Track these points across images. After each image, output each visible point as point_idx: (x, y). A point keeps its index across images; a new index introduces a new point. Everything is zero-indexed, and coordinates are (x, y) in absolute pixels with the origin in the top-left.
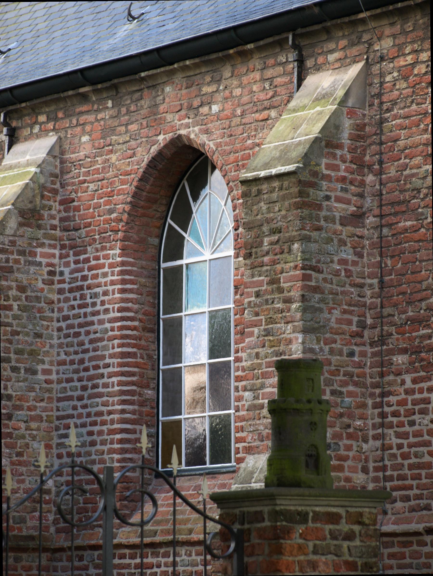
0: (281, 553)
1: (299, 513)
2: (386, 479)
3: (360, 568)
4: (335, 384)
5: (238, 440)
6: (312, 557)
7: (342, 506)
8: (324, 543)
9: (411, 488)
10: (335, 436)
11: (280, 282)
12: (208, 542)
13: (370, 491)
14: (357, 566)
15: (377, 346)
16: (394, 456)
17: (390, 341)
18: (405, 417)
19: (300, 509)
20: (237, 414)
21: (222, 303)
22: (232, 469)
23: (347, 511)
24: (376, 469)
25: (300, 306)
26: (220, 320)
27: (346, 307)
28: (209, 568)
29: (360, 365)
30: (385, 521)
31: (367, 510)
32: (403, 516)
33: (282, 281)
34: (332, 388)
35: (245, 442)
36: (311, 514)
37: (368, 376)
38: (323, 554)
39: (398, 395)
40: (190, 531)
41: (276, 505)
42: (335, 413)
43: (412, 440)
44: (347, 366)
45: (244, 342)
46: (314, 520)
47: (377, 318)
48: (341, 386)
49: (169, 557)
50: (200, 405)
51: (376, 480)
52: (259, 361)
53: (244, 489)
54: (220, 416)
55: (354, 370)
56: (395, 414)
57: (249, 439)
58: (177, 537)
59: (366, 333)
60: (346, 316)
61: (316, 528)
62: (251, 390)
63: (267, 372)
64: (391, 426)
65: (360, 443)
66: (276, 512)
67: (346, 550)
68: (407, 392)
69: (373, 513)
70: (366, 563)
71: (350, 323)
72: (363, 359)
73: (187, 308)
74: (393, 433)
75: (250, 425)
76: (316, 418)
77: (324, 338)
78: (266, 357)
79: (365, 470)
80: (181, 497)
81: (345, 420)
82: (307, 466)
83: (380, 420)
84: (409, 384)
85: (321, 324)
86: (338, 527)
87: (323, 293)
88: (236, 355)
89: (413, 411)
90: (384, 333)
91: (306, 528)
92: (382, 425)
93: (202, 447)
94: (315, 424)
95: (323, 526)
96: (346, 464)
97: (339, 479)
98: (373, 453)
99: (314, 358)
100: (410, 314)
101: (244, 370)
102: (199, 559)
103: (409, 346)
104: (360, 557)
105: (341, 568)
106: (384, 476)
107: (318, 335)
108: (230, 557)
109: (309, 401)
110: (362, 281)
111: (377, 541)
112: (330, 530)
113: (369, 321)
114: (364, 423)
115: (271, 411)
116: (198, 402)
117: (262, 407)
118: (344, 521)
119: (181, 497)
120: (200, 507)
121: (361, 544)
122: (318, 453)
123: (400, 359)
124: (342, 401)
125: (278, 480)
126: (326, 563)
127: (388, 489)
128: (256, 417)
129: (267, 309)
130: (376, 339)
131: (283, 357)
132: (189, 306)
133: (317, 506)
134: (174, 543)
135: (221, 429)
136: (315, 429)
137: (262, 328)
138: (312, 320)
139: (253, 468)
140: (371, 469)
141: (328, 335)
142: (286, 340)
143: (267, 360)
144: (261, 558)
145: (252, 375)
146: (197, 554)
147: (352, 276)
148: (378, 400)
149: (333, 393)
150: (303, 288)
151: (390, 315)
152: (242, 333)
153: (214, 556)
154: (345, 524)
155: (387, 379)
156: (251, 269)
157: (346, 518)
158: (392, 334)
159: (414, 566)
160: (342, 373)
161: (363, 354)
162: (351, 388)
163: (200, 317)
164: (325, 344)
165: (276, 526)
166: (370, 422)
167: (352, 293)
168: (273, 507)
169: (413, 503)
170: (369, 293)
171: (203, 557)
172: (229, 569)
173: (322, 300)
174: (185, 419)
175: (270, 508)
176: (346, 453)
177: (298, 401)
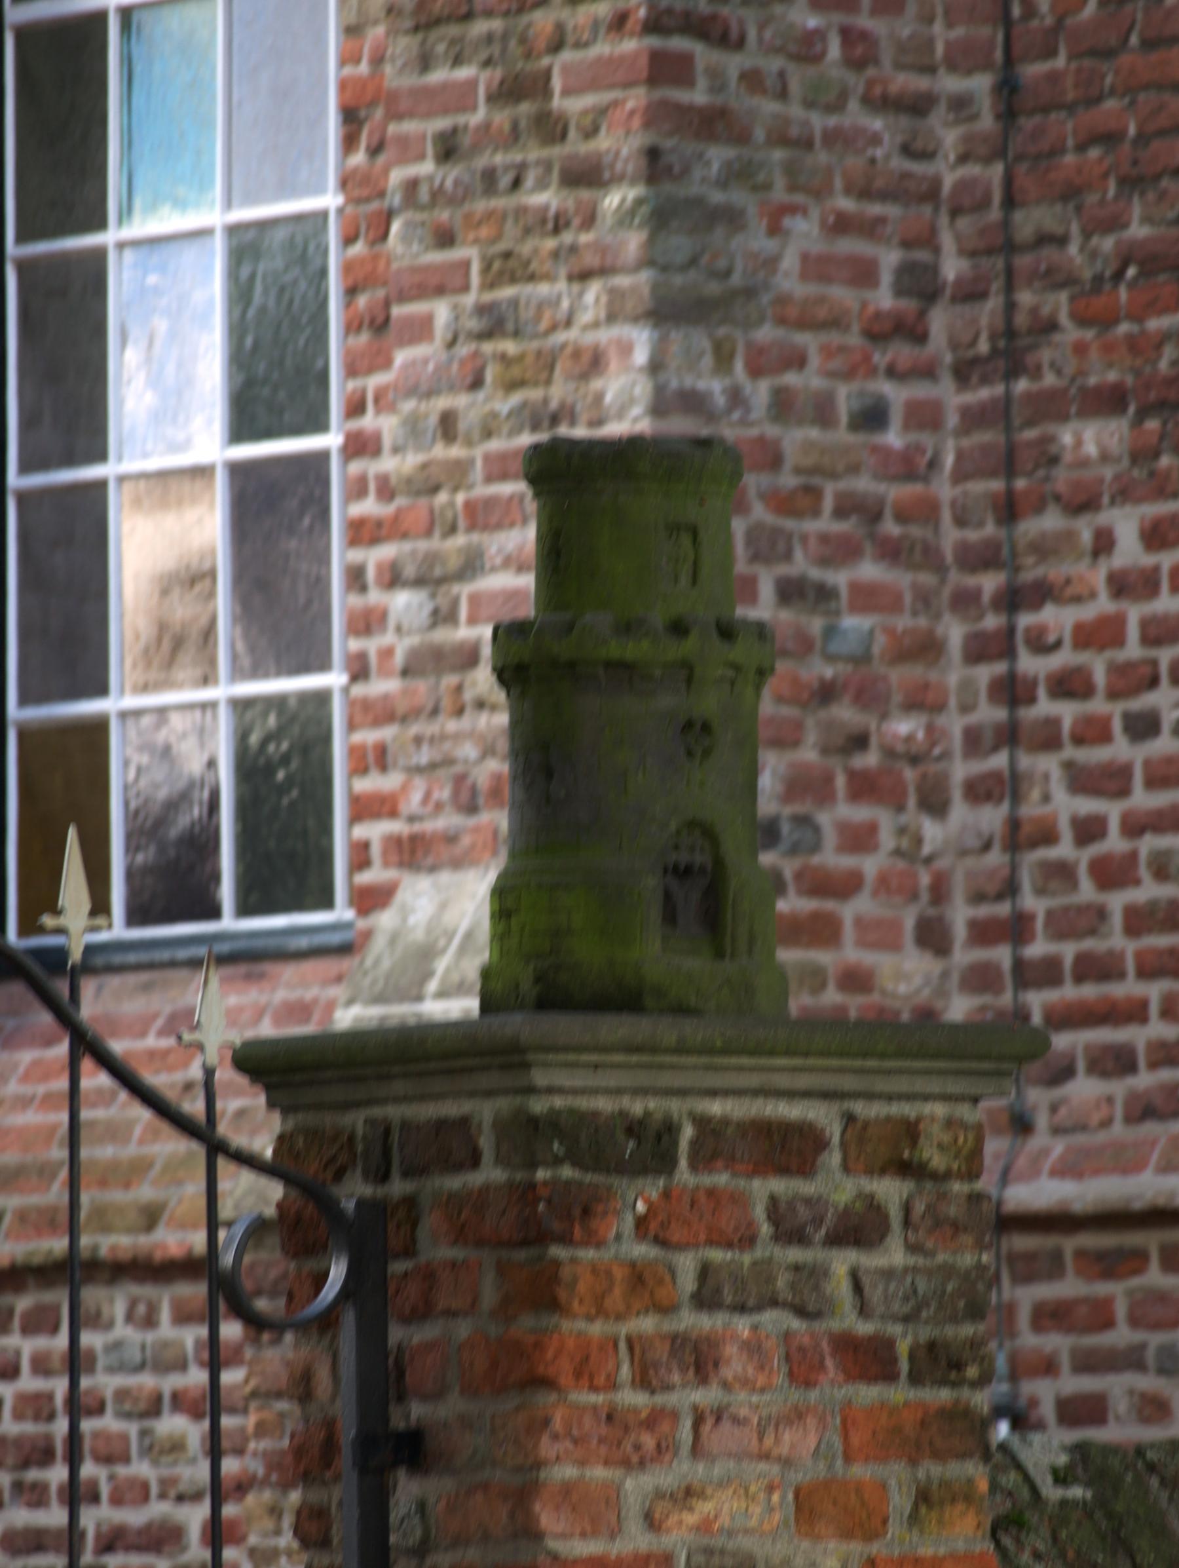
0: (554, 1305)
1: (635, 1128)
2: (1028, 975)
3: (904, 1366)
4: (798, 555)
5: (363, 808)
6: (690, 1321)
7: (827, 1095)
8: (747, 1259)
9: (1136, 1012)
10: (800, 785)
11: (547, 93)
12: (227, 1259)
13: (955, 1028)
14: (894, 1360)
15: (985, 380)
16: (1063, 873)
17: (1045, 355)
18: (1114, 694)
19: (637, 1107)
20: (359, 690)
21: (286, 190)
22: (335, 939)
23: (850, 1119)
24: (982, 933)
25: (639, 202)
26: (279, 263)
27: (846, 204)
28: (231, 1377)
29: (908, 467)
30: (1022, 1162)
31: (939, 1110)
32: (1101, 1137)
33: (557, 83)
34: (783, 570)
35: (393, 814)
36: (688, 1132)
37: (946, 516)
38: (741, 1308)
39: (1077, 599)
40: (151, 1217)
41: (531, 1090)
42: (796, 682)
43: (1142, 799)
44: (854, 469)
45: (387, 364)
46: (702, 1158)
47: (990, 252)
48: (824, 562)
49: (55, 1329)
50: (187, 656)
51: (981, 979)
52: (456, 451)
53: (393, 1023)
54: (278, 702)
55: (881, 488)
56: (1069, 685)
57: (414, 801)
58: (85, 1241)
59: (939, 321)
60: (849, 246)
61: (712, 1193)
62: (419, 582)
63: (490, 503)
64: (1048, 738)
65: (911, 814)
66: (533, 1123)
67: (839, 1286)
68: (1120, 586)
69: (964, 1126)
70: (932, 1346)
71: (863, 274)
72: (927, 440)
73: (126, 212)
74: (1056, 773)
75: (418, 740)
76: (709, 704)
77: (749, 345)
78: (488, 434)
79: (932, 937)
80: (106, 1061)
81: (845, 713)
82: (670, 916)
83: (1000, 714)
84: (1129, 550)
85: (736, 279)
86: (807, 1188)
87: (742, 138)
88: (355, 424)
89: (1146, 670)
90: (1021, 320)
91: (666, 1194)
92: (1009, 736)
93: (203, 843)
94: (706, 728)
95: (742, 1183)
96: (849, 911)
97: (816, 978)
98: (970, 862)
99: (705, 432)
100: (1138, 231)
101: (386, 491)
102: (192, 1336)
103: (1129, 380)
104: (906, 1319)
105: (822, 1366)
106: (1019, 965)
107: (722, 331)
108: (327, 1321)
109: (679, 628)
110: (922, 83)
111: (980, 1246)
112: (773, 1200)
113: (952, 268)
114: (930, 729)
115: (508, 674)
116: (178, 643)
117: (469, 657)
118: (834, 1158)
119: (106, 1061)
120: (195, 1107)
121: (911, 1261)
122: (719, 863)
123: (1090, 440)
124: (830, 632)
125: (538, 980)
126: (753, 1348)
127: (1037, 1019)
128: (446, 703)
129: (489, 215)
130: (983, 347)
131: (563, 431)
132: (138, 203)
133: (713, 1093)
134: (74, 1271)
135: (285, 760)
136: (707, 753)
137: (469, 300)
138: (693, 262)
139: (427, 932)
140: (960, 931)
141: (766, 333)
142: (577, 354)
143: (495, 445)
144: (463, 1329)
145: (423, 514)
146: (182, 1317)
147: (876, 61)
148: (992, 622)
149: (791, 592)
150: (654, 115)
151: (1044, 239)
152: (380, 324)
153: (255, 1323)
154: (838, 1175)
155: (1032, 527)
156: (416, 29)
157: (844, 1145)
158: (1051, 326)
159: (1150, 1356)
160: (828, 503)
161: (925, 417)
162: (870, 570)
163: (189, 254)
164: (755, 372)
165: (532, 1186)
166: (955, 724)
167: (875, 140)
168: (518, 1100)
169: (1144, 1080)
170: (950, 138)
171: (203, 1331)
172: (323, 1375)
173: (740, 174)
174: (124, 715)
175: (504, 1104)
176: (847, 862)
177: (627, 628)
